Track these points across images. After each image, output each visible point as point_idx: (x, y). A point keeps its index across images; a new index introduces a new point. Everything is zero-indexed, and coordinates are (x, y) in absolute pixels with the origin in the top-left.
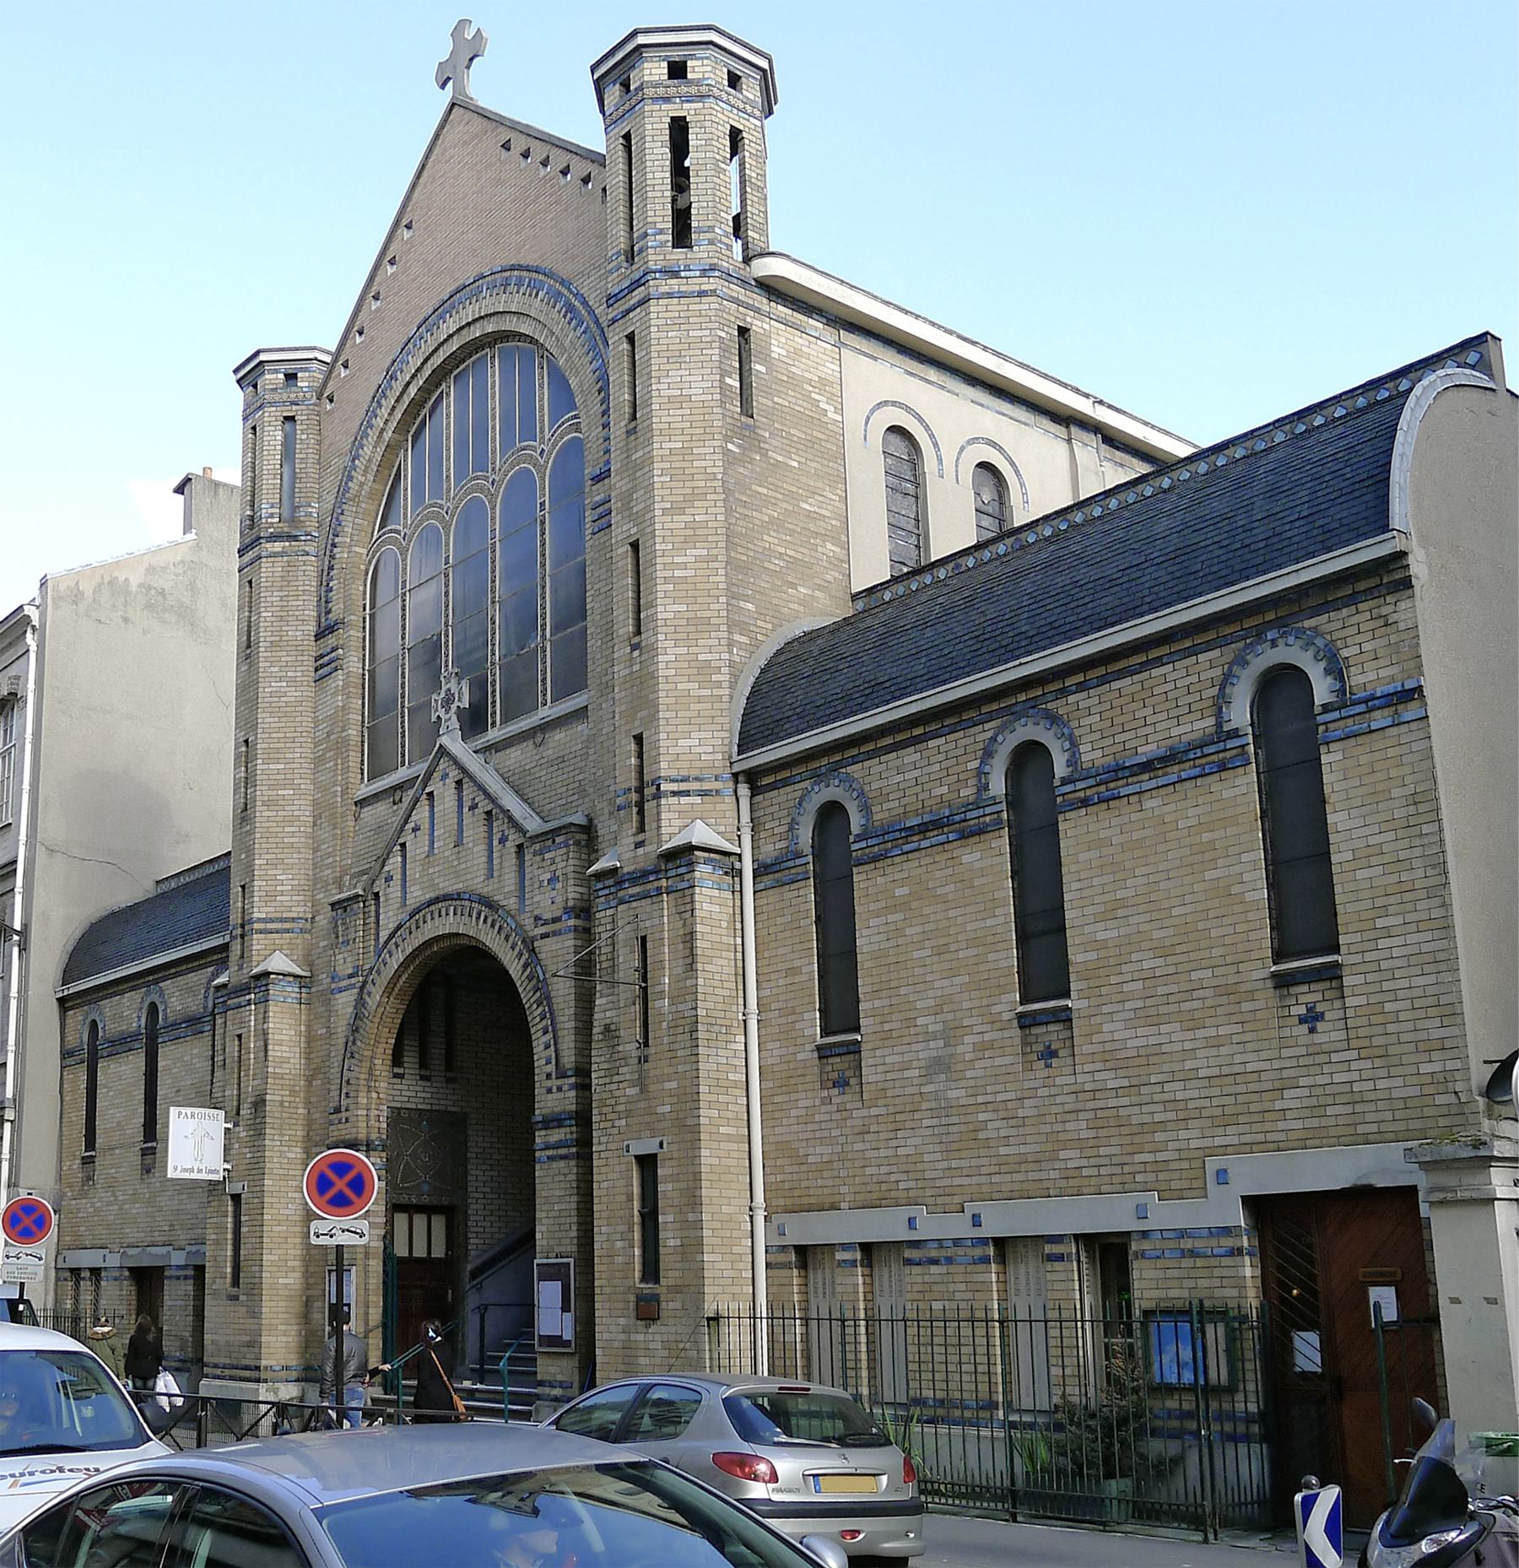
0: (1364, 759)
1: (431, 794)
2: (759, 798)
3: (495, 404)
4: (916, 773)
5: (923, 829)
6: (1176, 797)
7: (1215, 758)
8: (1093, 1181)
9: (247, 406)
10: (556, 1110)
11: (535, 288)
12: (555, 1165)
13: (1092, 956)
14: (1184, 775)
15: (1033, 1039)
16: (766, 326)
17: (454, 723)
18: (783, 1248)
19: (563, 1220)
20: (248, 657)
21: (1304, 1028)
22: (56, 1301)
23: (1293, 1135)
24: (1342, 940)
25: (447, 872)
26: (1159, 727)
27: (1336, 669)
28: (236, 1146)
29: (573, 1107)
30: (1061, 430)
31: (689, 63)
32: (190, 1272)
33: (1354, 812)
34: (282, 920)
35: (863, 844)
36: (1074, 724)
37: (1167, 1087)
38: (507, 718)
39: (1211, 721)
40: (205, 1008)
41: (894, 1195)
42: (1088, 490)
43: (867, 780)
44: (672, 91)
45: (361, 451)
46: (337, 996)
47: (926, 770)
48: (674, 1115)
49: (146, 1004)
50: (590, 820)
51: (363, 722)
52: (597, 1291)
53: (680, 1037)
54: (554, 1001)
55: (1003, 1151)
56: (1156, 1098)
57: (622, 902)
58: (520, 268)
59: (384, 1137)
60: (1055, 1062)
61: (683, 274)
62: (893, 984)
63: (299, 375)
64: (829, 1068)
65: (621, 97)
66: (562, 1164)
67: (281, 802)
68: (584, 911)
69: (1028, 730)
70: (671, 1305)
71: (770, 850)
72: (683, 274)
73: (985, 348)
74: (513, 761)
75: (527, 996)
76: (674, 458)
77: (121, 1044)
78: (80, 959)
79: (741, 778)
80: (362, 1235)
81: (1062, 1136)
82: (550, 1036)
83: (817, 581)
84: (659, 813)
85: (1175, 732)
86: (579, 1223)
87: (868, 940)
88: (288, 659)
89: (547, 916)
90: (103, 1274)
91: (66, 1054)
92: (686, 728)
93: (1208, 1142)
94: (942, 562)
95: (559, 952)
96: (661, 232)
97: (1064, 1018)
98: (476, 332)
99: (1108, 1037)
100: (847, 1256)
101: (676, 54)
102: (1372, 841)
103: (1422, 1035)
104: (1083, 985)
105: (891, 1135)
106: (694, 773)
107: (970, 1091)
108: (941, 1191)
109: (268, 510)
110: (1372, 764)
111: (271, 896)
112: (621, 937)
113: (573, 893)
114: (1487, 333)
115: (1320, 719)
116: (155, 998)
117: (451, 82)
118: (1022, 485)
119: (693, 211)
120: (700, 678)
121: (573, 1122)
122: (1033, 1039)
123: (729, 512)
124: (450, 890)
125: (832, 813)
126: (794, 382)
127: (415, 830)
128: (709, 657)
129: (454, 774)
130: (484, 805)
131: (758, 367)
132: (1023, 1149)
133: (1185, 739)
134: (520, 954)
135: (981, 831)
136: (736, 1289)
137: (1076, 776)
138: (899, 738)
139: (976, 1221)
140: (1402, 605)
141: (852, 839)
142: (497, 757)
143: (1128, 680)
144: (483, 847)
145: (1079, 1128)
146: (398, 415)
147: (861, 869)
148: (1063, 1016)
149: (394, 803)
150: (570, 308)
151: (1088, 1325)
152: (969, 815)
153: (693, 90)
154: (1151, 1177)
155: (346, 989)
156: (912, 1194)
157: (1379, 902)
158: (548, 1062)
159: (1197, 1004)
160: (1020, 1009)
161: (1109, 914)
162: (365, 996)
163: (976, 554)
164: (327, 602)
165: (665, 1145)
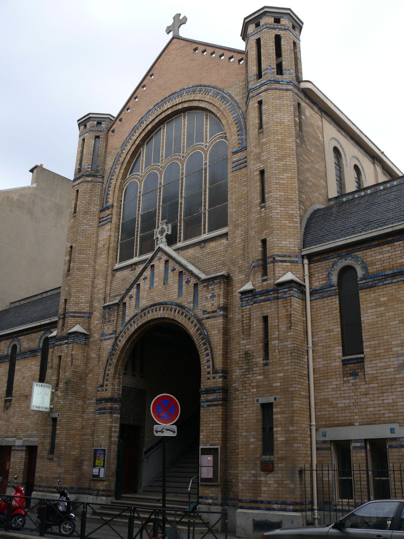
1: (153, 266)
2: (312, 265)
4: (389, 254)
5: (394, 275)
10: (212, 386)
12: (211, 408)
17: (164, 240)
18: (325, 442)
25: (160, 294)
28: (56, 399)
29: (221, 385)
31: (281, 19)
38: (185, 239)
40: (39, 346)
42: (380, 181)
43: (365, 257)
44: (276, 27)
45: (125, 147)
46: (104, 342)
49: (12, 345)
51: (118, 241)
54: (212, 343)
57: (255, 302)
58: (201, 86)
59: (121, 397)
61: (281, 83)
63: (102, 123)
64: (348, 369)
65: (255, 28)
67: (83, 269)
69: (348, 262)
71: (317, 284)
72: (281, 83)
74: (190, 254)
76: (278, 142)
79: (305, 257)
80: (174, 432)
82: (209, 357)
84: (274, 269)
86: (222, 432)
88: (90, 218)
89: (210, 310)
92: (284, 237)
94: (349, 194)
96: (273, 69)
100: (358, 445)
101: (277, 16)
106: (288, 254)
109: (86, 165)
111: (77, 304)
116: (16, 342)
117: (172, 32)
120: (289, 219)
121: (221, 391)
123: (298, 163)
124: (161, 301)
126: (312, 125)
127: (145, 279)
128: (293, 212)
129: (165, 258)
130: (178, 269)
134: (195, 326)
146: (143, 135)
147: (363, 291)
149: (132, 270)
153: (283, 27)
155: (109, 339)
158: (209, 367)
160: (343, 358)
163: (384, 185)
164: (106, 199)
165: (277, 399)
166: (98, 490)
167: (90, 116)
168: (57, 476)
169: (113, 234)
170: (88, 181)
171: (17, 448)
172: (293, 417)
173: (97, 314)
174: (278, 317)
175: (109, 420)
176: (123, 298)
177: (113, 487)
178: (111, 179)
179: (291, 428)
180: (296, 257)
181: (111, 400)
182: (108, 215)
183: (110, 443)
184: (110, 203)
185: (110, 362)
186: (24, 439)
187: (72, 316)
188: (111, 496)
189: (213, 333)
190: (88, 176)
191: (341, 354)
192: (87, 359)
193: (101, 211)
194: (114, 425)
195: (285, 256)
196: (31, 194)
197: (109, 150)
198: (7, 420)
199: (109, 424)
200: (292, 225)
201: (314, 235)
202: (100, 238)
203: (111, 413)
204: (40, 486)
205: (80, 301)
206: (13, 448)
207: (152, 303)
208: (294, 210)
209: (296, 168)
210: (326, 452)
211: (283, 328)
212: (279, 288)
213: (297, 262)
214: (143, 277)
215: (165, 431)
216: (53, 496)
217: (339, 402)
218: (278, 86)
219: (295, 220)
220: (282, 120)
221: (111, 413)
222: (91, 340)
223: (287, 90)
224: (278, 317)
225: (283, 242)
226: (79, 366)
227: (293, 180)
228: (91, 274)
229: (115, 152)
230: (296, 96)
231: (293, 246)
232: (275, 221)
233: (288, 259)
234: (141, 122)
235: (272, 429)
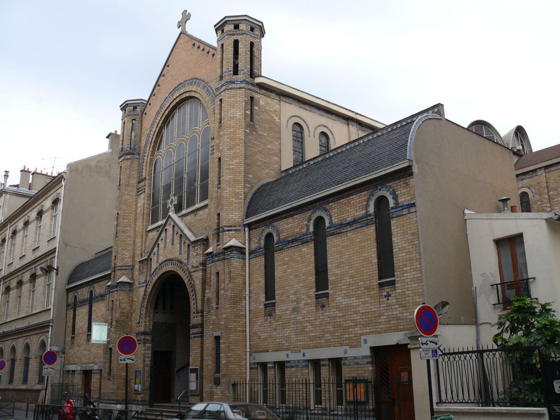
0: (401, 223)
1: (166, 229)
2: (251, 231)
3: (188, 116)
4: (291, 225)
5: (293, 241)
6: (356, 233)
7: (365, 222)
8: (333, 343)
9: (123, 116)
11: (199, 85)
12: (195, 339)
13: (334, 278)
14: (358, 227)
15: (319, 302)
16: (259, 96)
17: (173, 209)
18: (254, 363)
19: (197, 355)
20: (120, 189)
21: (386, 299)
22: (63, 380)
23: (383, 329)
24: (396, 274)
26: (352, 213)
27: (395, 198)
30: (346, 122)
32: (99, 372)
33: (399, 238)
34: (126, 266)
35: (277, 245)
36: (331, 211)
37: (352, 316)
38: (188, 207)
39: (364, 211)
41: (283, 347)
42: (354, 137)
44: (235, 33)
47: (294, 224)
48: (225, 325)
50: (208, 238)
52: (204, 376)
53: (227, 302)
55: (311, 334)
56: (350, 319)
57: (213, 262)
58: (196, 79)
60: (324, 309)
62: (284, 286)
64: (267, 311)
66: (197, 339)
68: (204, 264)
70: (223, 380)
71: (253, 247)
73: (323, 100)
75: (189, 290)
77: (83, 303)
78: (72, 278)
80: (133, 360)
81: (326, 330)
82: (195, 301)
83: (271, 168)
85: (356, 214)
87: (278, 273)
89: (195, 266)
90: (76, 372)
91: (68, 305)
92: (231, 211)
93: (362, 332)
95: (197, 276)
96: (230, 71)
97: (327, 295)
98: (184, 96)
99: (338, 301)
102: (403, 246)
103: (414, 301)
104: (332, 286)
105: (283, 330)
106: (233, 224)
107: (303, 317)
108: (295, 346)
110: (403, 224)
111: (123, 259)
112: (212, 272)
113: (201, 259)
114: (439, 104)
115: (391, 211)
116: (92, 289)
117: (181, 27)
118: (334, 138)
119: (239, 65)
122: (319, 302)
123: (245, 149)
124: (170, 258)
125: (269, 236)
126: (266, 111)
127: (162, 240)
129: (172, 223)
130: (180, 233)
131: (256, 108)
132: (316, 334)
133: (358, 216)
134: (188, 277)
135: (307, 242)
136: (241, 376)
137: (331, 226)
138: (287, 215)
139: (304, 355)
140: (411, 180)
141: (274, 244)
142: (185, 218)
143: (344, 200)
144: (179, 245)
145: (330, 328)
146: (163, 119)
147: (276, 252)
148: (327, 295)
150: (208, 90)
151: (331, 385)
152: (305, 237)
153: (240, 32)
154: (348, 342)
155: (142, 287)
156: (288, 347)
157: (404, 263)
158: (194, 309)
159: (360, 292)
161: (339, 265)
162: (147, 289)
166: (138, 401)
167: (227, 19)
168: (112, 391)
169: (146, 201)
170: (128, 159)
171: (95, 372)
172: (229, 346)
173: (137, 266)
174: (224, 273)
175: (143, 348)
176: (150, 255)
177: (147, 398)
178: (144, 156)
179: (229, 354)
180: (240, 226)
181: (144, 333)
182: (143, 187)
183: (144, 366)
184: (143, 177)
185: (143, 304)
186: (99, 364)
187: (119, 270)
188: (146, 405)
189: (197, 283)
190: (128, 154)
191: (264, 299)
192: (132, 301)
193: (139, 182)
194: (147, 352)
195: (231, 226)
196: (107, 158)
197: (143, 130)
198: (89, 350)
199: (143, 352)
200: (238, 201)
201: (383, 160)
202: (139, 205)
203: (144, 343)
204: (104, 400)
205: (125, 257)
206: (93, 372)
207: (165, 259)
208: (240, 190)
209: (243, 155)
210: (255, 370)
211: (227, 282)
212: (225, 251)
213: (240, 230)
214: (160, 239)
215: (127, 360)
216: (110, 407)
217: (262, 335)
218: (233, 86)
219: (240, 197)
220: (235, 115)
221: (144, 343)
222: (134, 287)
223: (240, 88)
224: (224, 273)
225: (230, 216)
226: (125, 308)
227: (240, 164)
228: (132, 235)
229: (147, 132)
230: (249, 91)
231: (238, 217)
232: (225, 199)
233: (233, 228)
234: (161, 108)
235: (219, 354)
